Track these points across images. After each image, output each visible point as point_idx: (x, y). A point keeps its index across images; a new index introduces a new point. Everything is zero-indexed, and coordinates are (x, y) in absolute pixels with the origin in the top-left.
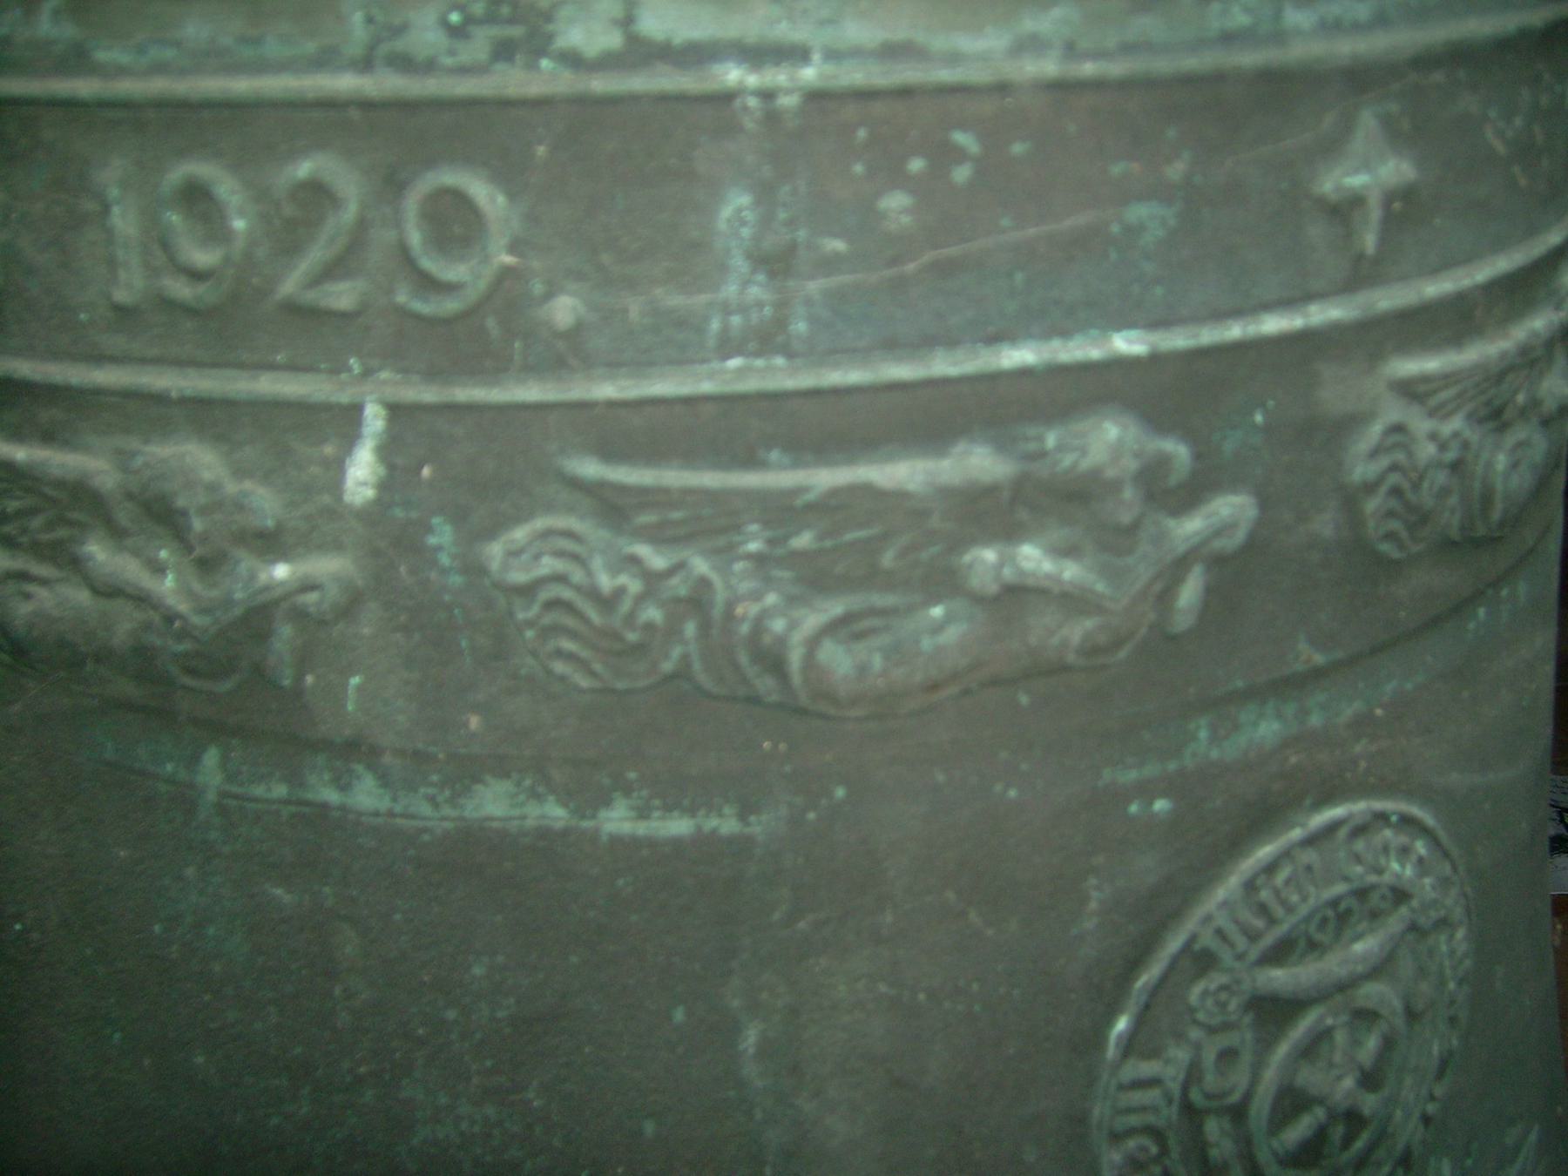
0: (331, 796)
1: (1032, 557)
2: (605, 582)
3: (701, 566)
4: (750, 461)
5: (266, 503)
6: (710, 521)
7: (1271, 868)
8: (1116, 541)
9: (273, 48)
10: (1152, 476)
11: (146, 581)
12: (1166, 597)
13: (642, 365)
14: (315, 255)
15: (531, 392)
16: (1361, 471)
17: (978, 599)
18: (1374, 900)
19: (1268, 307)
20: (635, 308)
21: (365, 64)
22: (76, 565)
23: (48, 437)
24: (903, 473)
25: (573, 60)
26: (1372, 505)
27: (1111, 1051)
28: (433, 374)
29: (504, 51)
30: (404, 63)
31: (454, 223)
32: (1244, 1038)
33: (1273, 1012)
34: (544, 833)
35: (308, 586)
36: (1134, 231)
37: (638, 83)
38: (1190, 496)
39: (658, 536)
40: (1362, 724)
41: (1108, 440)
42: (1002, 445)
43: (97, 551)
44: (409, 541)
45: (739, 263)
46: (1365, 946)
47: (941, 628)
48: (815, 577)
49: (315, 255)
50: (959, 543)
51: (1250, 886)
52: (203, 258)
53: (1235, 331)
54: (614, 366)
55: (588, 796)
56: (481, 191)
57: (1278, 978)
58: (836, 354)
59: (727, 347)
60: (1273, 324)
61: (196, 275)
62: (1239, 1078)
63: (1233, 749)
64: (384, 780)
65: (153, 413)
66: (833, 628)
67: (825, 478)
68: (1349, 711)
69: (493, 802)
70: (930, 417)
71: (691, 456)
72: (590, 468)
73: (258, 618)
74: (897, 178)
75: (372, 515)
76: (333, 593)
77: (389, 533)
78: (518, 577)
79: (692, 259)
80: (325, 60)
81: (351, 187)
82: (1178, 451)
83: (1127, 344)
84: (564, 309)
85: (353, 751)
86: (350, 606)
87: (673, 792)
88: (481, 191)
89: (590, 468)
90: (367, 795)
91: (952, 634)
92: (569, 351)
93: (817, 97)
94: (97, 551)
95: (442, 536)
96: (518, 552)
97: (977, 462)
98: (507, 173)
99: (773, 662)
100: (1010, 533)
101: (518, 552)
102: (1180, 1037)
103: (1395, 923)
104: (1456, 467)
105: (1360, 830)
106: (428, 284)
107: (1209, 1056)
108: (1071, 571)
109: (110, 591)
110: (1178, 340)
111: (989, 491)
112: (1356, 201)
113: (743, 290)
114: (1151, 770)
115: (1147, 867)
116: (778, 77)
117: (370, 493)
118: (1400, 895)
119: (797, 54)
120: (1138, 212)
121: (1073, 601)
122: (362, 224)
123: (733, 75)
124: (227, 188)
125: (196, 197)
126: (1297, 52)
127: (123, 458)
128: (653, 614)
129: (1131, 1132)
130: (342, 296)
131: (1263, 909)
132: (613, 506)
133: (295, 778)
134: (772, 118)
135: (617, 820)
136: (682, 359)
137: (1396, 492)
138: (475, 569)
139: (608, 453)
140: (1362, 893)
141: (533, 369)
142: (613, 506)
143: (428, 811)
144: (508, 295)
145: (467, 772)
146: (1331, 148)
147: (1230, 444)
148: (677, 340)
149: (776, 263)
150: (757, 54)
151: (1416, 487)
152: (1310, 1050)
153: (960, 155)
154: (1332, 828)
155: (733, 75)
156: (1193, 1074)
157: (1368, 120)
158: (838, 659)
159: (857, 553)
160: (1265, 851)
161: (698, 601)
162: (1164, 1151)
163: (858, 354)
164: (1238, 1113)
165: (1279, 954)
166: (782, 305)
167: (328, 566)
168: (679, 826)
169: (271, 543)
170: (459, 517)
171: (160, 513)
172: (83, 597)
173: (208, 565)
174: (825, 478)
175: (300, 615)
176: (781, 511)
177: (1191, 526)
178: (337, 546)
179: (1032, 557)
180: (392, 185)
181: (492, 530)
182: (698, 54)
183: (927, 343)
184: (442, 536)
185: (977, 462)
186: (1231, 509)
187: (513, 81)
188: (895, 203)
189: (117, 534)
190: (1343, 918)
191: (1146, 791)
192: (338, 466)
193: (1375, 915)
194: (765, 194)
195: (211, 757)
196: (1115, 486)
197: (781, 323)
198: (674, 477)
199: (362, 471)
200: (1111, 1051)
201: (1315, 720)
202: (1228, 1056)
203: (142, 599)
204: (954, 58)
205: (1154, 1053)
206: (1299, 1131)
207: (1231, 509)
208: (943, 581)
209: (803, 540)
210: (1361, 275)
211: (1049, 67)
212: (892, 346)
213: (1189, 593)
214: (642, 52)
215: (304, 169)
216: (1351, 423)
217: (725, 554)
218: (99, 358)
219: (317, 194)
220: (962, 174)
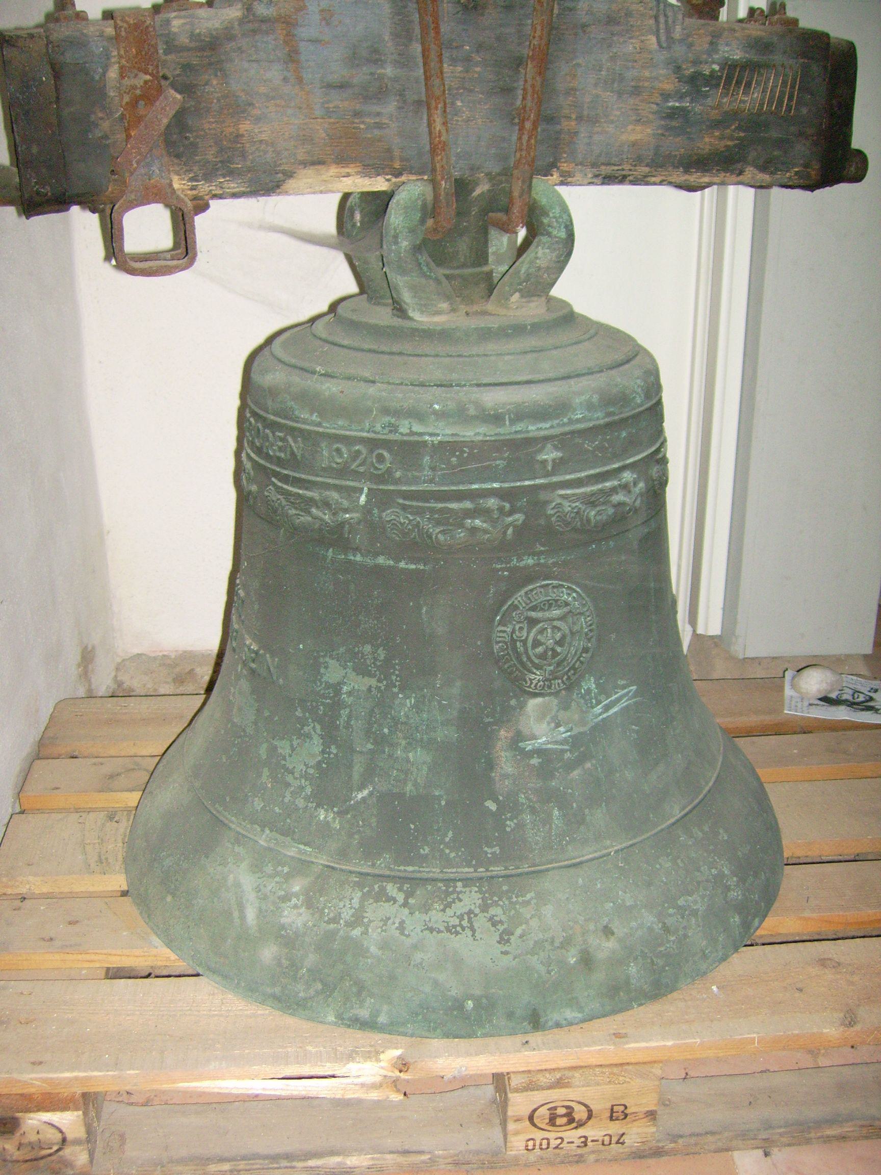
0: (352, 558)
1: (478, 522)
2: (402, 521)
3: (418, 519)
4: (428, 501)
5: (346, 503)
6: (420, 512)
7: (532, 590)
8: (493, 522)
9: (353, 427)
10: (501, 509)
11: (323, 516)
12: (505, 533)
13: (410, 484)
14: (358, 462)
15: (392, 488)
16: (550, 512)
17: (467, 529)
18: (559, 603)
19: (526, 480)
20: (410, 474)
21: (368, 432)
22: (309, 513)
23: (306, 489)
24: (454, 506)
25: (402, 434)
26: (553, 519)
27: (496, 623)
28: (376, 483)
29: (391, 432)
30: (375, 432)
31: (381, 459)
32: (525, 626)
33: (532, 622)
34: (389, 567)
35: (352, 519)
36: (497, 466)
37: (411, 438)
38: (510, 513)
39: (411, 513)
40: (554, 564)
41: (492, 502)
42: (472, 502)
43: (314, 510)
44: (370, 512)
45: (427, 468)
46: (556, 613)
47: (461, 534)
48: (438, 523)
49: (358, 462)
50: (464, 518)
51: (526, 593)
52: (339, 461)
53: (518, 484)
54: (406, 484)
55: (397, 560)
56: (386, 454)
57: (533, 614)
58: (443, 485)
59: (425, 482)
60: (527, 483)
61: (338, 464)
62: (524, 633)
63: (522, 564)
64: (362, 555)
65: (327, 486)
66: (440, 532)
67: (440, 505)
68: (551, 561)
69: (381, 560)
70: (460, 496)
71: (418, 500)
72: (401, 501)
73: (342, 525)
74: (454, 455)
75: (364, 507)
76: (356, 520)
77: (367, 510)
78: (388, 519)
79: (420, 468)
80: (362, 430)
81: (364, 451)
82: (507, 506)
83: (496, 485)
84: (398, 474)
85: (356, 550)
86: (359, 523)
87: (412, 560)
88: (386, 454)
89: (401, 501)
90: (358, 558)
91: (462, 535)
92: (397, 482)
93: (440, 442)
94: (314, 510)
95: (376, 511)
96: (388, 515)
97: (468, 505)
98: (390, 451)
99: (430, 537)
100: (473, 518)
101: (388, 515)
102: (510, 623)
103: (566, 610)
104: (577, 513)
105: (554, 587)
106: (376, 469)
107: (517, 627)
108: (485, 525)
109: (315, 518)
110: (506, 485)
111: (469, 510)
112: (546, 461)
113: (427, 472)
114: (503, 566)
115: (503, 586)
116: (434, 439)
117: (255, 922)
118: (567, 604)
119: (438, 435)
120: (498, 462)
121: (486, 531)
122: (366, 458)
123: (427, 438)
124: (344, 450)
125: (338, 450)
126: (530, 435)
127: (320, 494)
128: (410, 527)
129: (500, 642)
130: (362, 469)
131: (529, 599)
132: (404, 508)
133: (346, 554)
134: (433, 445)
135: (402, 565)
136: (417, 484)
137: (558, 516)
138: (380, 517)
139: (404, 499)
140: (556, 601)
141: (392, 484)
142: (404, 508)
143: (369, 561)
144: (389, 471)
145: (376, 555)
146: (540, 451)
147: (519, 504)
148: (416, 480)
149: (433, 469)
150: (431, 435)
151: (565, 516)
152: (542, 631)
153: (465, 452)
154: (548, 585)
155: (427, 438)
156: (513, 632)
157: (549, 446)
158: (441, 538)
159: (445, 519)
160: (531, 587)
161: (417, 525)
162: (507, 647)
163: (448, 485)
164: (524, 642)
165: (534, 609)
166: (434, 476)
167: (356, 515)
168: (413, 567)
169: (346, 511)
170: (378, 508)
171: (326, 504)
172: (310, 519)
173: (334, 514)
174: (440, 505)
175: (349, 523)
176: (432, 511)
177: (510, 519)
178: (357, 512)
179: (478, 522)
180: (371, 451)
181: (384, 511)
182: (421, 434)
183: (459, 483)
184: (376, 511)
185: (468, 505)
186: (519, 517)
187: (392, 437)
188: (454, 459)
189: (318, 507)
190: (550, 605)
191: (503, 570)
192: (359, 498)
193: (560, 606)
194: (432, 457)
195: (331, 550)
196: (493, 510)
197: (434, 479)
198: (414, 503)
199: (363, 499)
200: (496, 623)
201: (542, 561)
202: (521, 629)
203: (322, 520)
204: (464, 436)
205: (505, 625)
206: (540, 650)
207: (519, 517)
208: (462, 526)
209: (436, 516)
210: (547, 475)
211: (480, 438)
212: (453, 484)
213: (510, 531)
214: (412, 433)
215: (357, 448)
216: (547, 502)
217: (422, 518)
218: (317, 476)
219: (358, 452)
220: (465, 455)
